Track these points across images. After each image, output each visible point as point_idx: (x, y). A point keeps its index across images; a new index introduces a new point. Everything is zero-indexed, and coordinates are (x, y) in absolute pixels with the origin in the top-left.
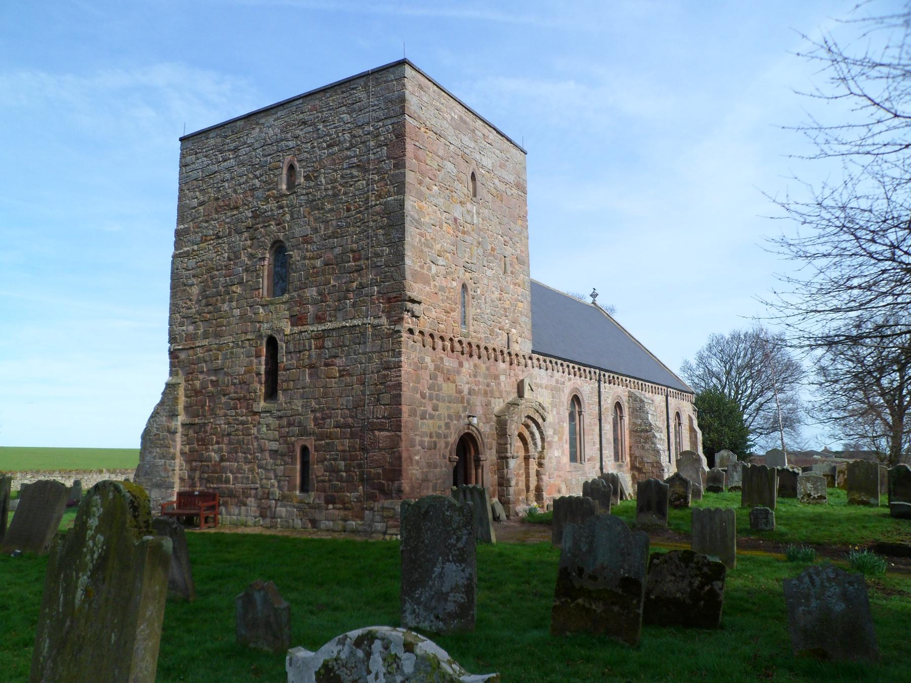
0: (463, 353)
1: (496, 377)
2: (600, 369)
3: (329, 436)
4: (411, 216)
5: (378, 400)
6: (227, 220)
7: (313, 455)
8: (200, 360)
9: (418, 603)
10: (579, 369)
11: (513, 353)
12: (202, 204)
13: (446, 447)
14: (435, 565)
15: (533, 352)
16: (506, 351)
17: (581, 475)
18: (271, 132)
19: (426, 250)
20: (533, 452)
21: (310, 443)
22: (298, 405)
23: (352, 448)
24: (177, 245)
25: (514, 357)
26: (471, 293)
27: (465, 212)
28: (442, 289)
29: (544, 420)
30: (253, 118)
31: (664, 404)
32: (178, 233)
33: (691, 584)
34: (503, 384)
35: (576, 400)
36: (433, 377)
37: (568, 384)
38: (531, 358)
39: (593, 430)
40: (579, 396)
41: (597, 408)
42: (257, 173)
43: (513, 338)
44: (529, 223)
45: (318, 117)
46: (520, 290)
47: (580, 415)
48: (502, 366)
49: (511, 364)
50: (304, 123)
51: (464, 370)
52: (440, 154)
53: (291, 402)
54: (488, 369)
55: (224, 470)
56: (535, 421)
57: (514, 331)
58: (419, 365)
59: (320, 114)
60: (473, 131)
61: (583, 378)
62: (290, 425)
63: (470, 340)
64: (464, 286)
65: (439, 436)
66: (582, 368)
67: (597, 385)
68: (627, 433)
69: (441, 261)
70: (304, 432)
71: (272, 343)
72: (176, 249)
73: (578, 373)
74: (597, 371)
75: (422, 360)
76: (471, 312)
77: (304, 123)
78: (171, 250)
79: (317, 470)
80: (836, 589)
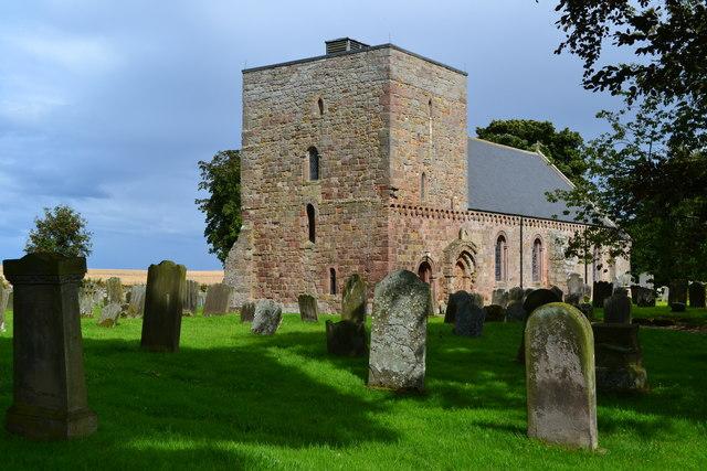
1: (444, 228)
7: (338, 273)
20: (468, 273)
22: (328, 245)
28: (410, 179)
32: (244, 135)
36: (406, 231)
64: (423, 174)
68: (545, 260)
71: (311, 209)
76: (428, 189)
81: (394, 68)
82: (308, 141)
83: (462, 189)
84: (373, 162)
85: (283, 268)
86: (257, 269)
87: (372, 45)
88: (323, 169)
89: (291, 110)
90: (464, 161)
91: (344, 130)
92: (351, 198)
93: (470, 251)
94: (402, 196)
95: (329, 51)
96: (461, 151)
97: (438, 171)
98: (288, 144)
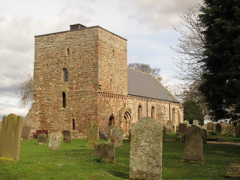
0: (111, 97)
1: (119, 102)
2: (147, 98)
5: (92, 108)
6: (50, 61)
7: (76, 121)
8: (43, 97)
10: (141, 98)
12: (42, 55)
15: (128, 95)
16: (121, 95)
18: (62, 39)
19: (102, 73)
20: (128, 120)
21: (75, 118)
22: (71, 109)
23: (86, 119)
28: (106, 82)
29: (131, 112)
31: (169, 107)
32: (35, 63)
34: (120, 104)
37: (138, 102)
38: (127, 96)
41: (146, 109)
44: (127, 60)
45: (75, 37)
46: (125, 79)
49: (122, 98)
54: (116, 100)
56: (128, 113)
58: (101, 101)
65: (105, 117)
66: (142, 98)
67: (146, 102)
68: (156, 115)
69: (106, 75)
71: (64, 94)
74: (147, 98)
76: (112, 86)
79: (77, 125)
81: (100, 36)
82: (63, 66)
83: (125, 86)
84: (91, 74)
85: (52, 119)
86: (40, 120)
87: (87, 25)
88: (70, 77)
89: (55, 53)
90: (126, 75)
91: (79, 61)
92: (81, 89)
93: (129, 112)
94: (103, 88)
95: (71, 29)
96: (125, 71)
97: (117, 77)
98: (54, 67)
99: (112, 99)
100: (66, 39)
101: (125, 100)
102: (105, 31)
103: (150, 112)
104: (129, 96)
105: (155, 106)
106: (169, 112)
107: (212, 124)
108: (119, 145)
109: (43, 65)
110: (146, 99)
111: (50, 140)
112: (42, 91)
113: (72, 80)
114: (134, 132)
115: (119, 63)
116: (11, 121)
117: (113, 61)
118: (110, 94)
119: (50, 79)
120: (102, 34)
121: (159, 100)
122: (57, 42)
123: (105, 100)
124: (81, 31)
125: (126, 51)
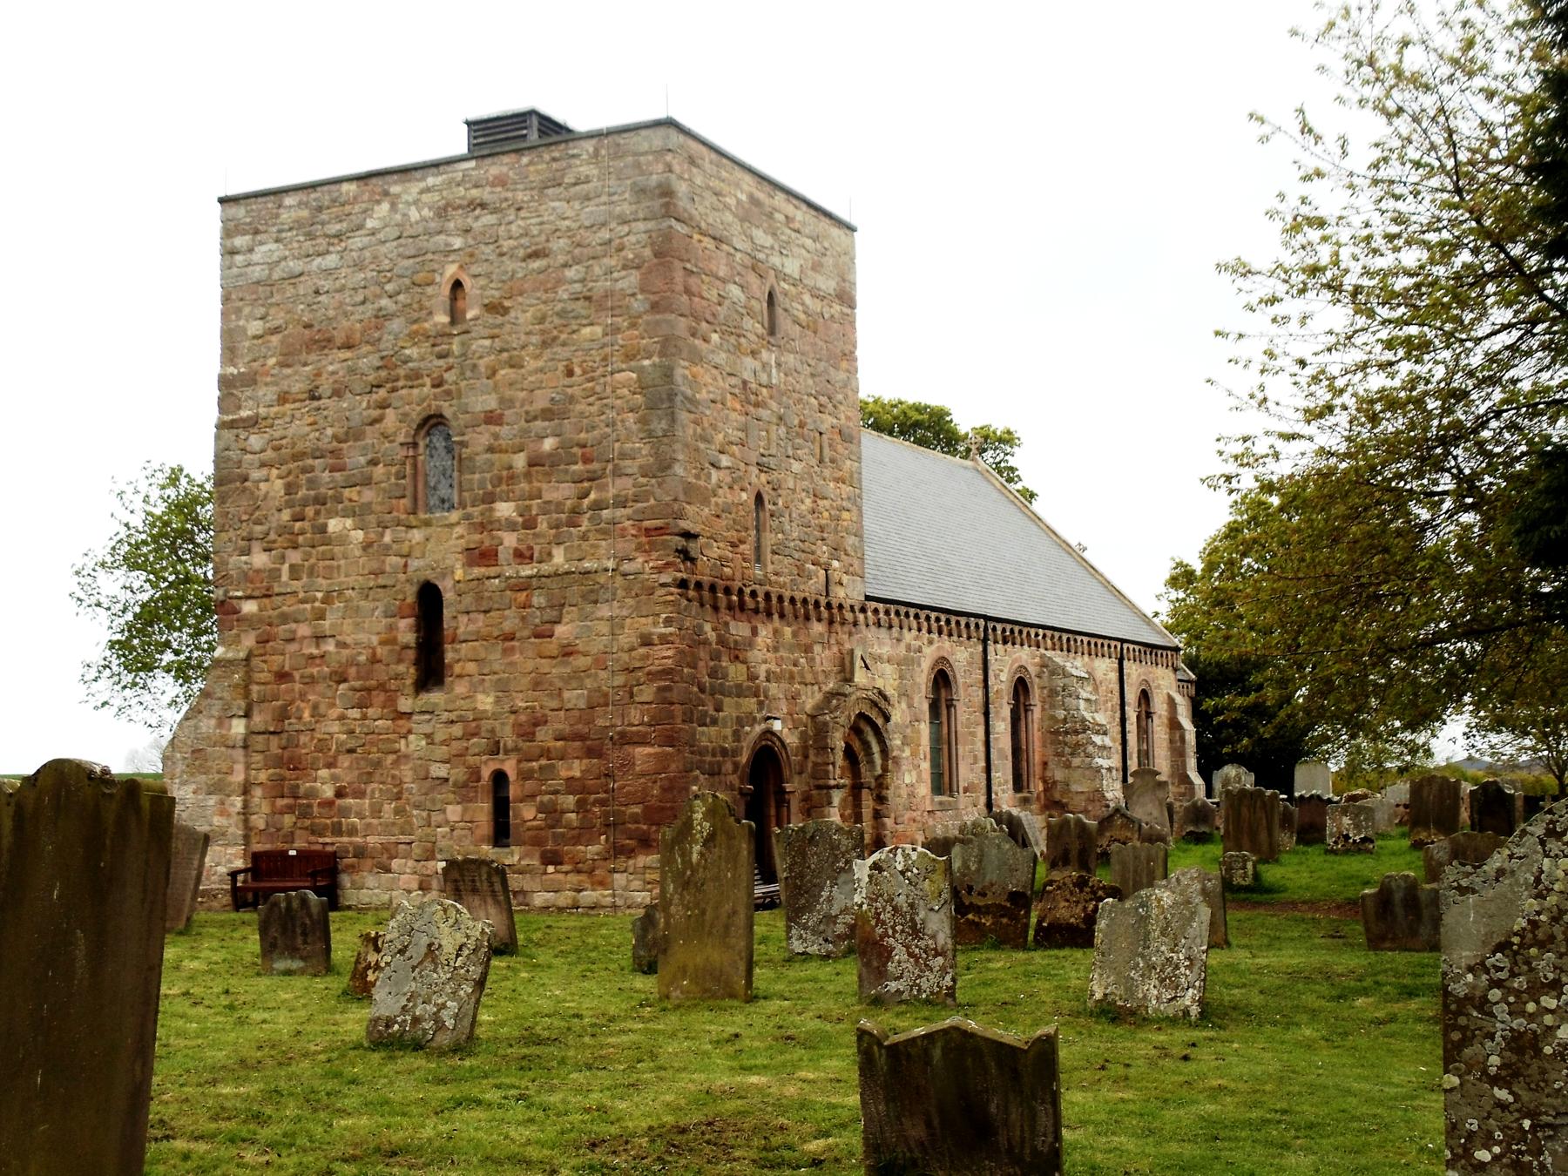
1: (808, 649)
3: (546, 753)
4: (683, 394)
5: (632, 695)
9: (805, 928)
11: (835, 603)
13: (735, 772)
14: (822, 889)
16: (823, 601)
17: (951, 818)
19: (702, 446)
20: (867, 778)
21: (510, 767)
22: (485, 702)
24: (224, 404)
25: (835, 611)
26: (769, 506)
27: (759, 368)
28: (727, 509)
29: (887, 719)
30: (374, 181)
31: (1114, 676)
32: (225, 383)
33: (1085, 908)
35: (942, 679)
37: (927, 650)
38: (863, 610)
39: (973, 734)
40: (950, 673)
42: (389, 287)
43: (835, 576)
47: (949, 707)
48: (818, 628)
49: (831, 622)
50: (483, 205)
51: (759, 640)
52: (721, 274)
53: (475, 693)
54: (795, 634)
55: (345, 812)
56: (869, 725)
57: (835, 564)
59: (510, 195)
60: (770, 216)
61: (955, 638)
62: (468, 735)
63: (768, 588)
64: (759, 499)
65: (724, 752)
67: (980, 648)
70: (495, 749)
71: (429, 600)
72: (222, 410)
73: (945, 629)
75: (698, 630)
76: (769, 539)
77: (483, 205)
78: (213, 414)
80: (1197, 886)
81: (682, 188)
85: (346, 770)
89: (369, 309)
93: (873, 715)
99: (765, 634)
100: (442, 212)
101: (850, 634)
102: (714, 156)
103: (1006, 711)
104: (876, 611)
105: (1033, 670)
106: (1118, 715)
107: (1441, 790)
108: (924, 986)
109: (283, 399)
110: (977, 626)
111: (388, 959)
112: (274, 574)
113: (490, 499)
114: (1478, 968)
115: (810, 382)
116: (68, 795)
117: (764, 367)
118: (754, 594)
119: (330, 492)
120: (698, 181)
121: (1057, 634)
122: (381, 236)
123: (719, 636)
124: (547, 157)
125: (846, 298)
